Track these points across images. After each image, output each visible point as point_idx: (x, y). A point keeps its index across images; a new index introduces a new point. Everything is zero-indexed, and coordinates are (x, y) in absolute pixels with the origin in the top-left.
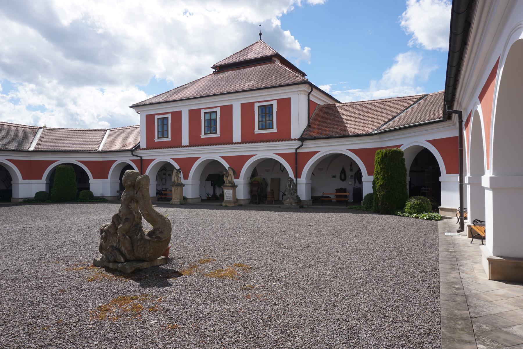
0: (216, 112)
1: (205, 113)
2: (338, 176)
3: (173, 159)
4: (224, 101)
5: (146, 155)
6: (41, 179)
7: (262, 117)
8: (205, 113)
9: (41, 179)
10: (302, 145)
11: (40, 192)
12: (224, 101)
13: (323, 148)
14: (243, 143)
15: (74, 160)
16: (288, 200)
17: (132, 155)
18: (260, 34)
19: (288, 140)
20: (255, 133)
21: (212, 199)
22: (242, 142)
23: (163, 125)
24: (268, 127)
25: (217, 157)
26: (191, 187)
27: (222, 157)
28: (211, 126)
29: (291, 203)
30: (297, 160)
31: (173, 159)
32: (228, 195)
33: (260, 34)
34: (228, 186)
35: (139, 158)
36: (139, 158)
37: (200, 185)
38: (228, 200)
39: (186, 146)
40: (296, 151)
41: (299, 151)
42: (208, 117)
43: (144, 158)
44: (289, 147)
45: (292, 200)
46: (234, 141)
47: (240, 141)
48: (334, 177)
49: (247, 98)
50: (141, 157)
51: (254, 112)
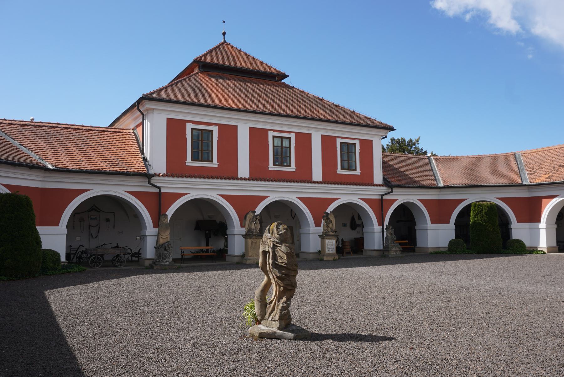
0: (290, 138)
1: (274, 137)
2: (348, 224)
3: (222, 196)
4: (227, 119)
5: (169, 186)
6: (448, 223)
7: (286, 153)
8: (274, 137)
9: (57, 225)
10: (392, 192)
11: (50, 250)
12: (303, 127)
13: (401, 197)
14: (253, 180)
15: (492, 197)
16: (394, 249)
17: (149, 183)
18: (224, 34)
19: (234, 179)
20: (338, 173)
21: (352, 251)
22: (251, 178)
23: (348, 152)
24: (200, 159)
25: (355, 200)
26: (376, 234)
27: (419, 200)
28: (281, 157)
29: (396, 251)
30: (380, 206)
31: (419, 200)
32: (330, 247)
33: (224, 34)
34: (333, 236)
35: (157, 190)
36: (157, 190)
37: (455, 230)
38: (330, 252)
39: (245, 179)
40: (382, 197)
41: (384, 197)
42: (278, 142)
43: (163, 191)
44: (374, 193)
45: (398, 249)
46: (239, 177)
47: (248, 176)
48: (345, 225)
49: (261, 122)
50: (159, 188)
51: (186, 135)
